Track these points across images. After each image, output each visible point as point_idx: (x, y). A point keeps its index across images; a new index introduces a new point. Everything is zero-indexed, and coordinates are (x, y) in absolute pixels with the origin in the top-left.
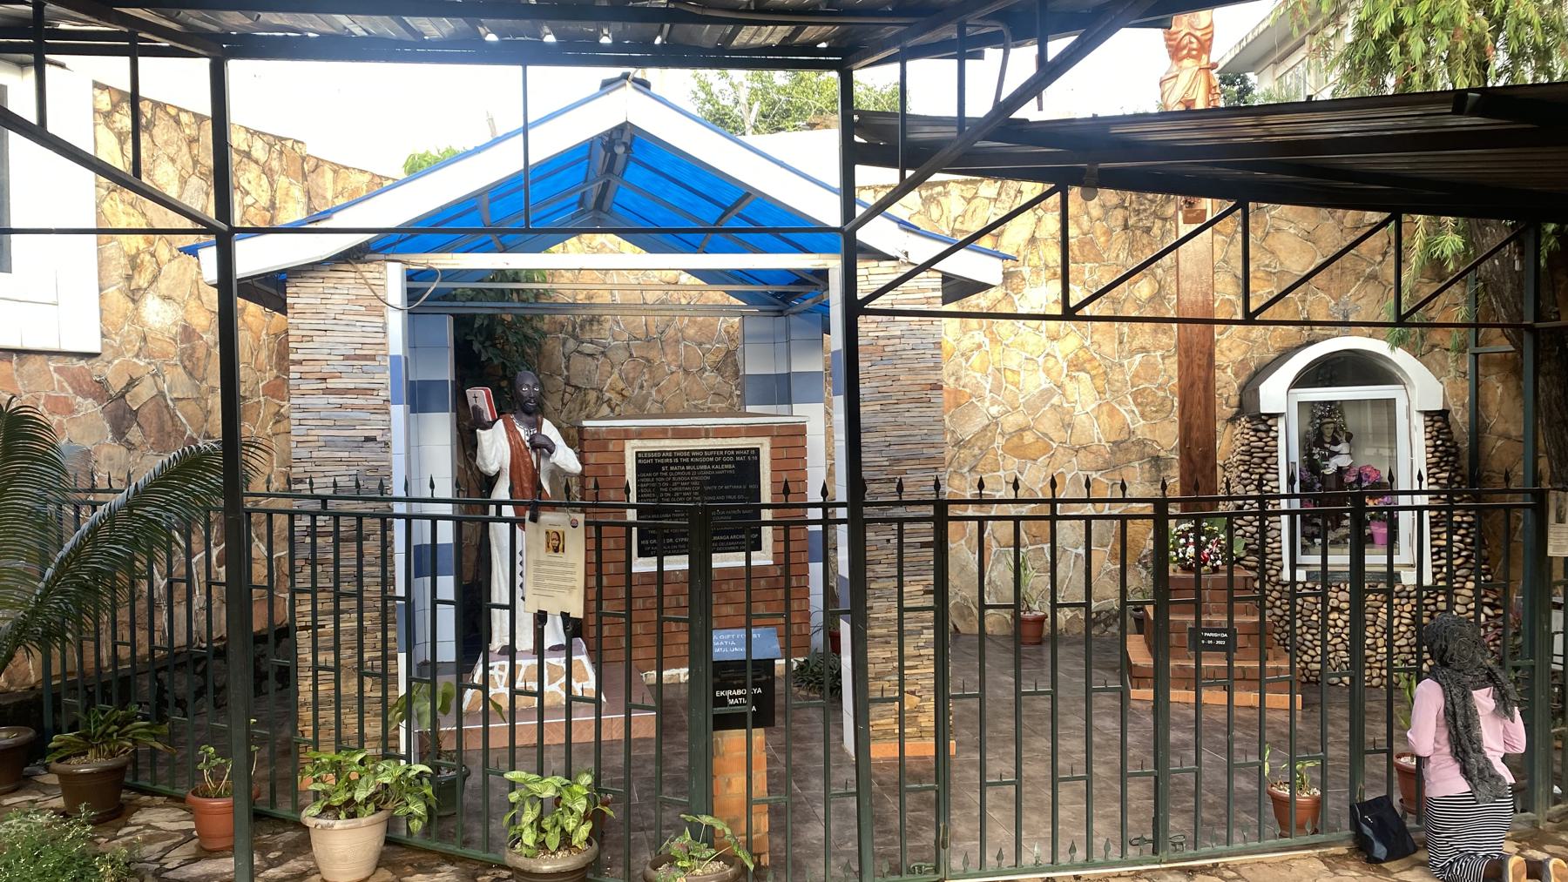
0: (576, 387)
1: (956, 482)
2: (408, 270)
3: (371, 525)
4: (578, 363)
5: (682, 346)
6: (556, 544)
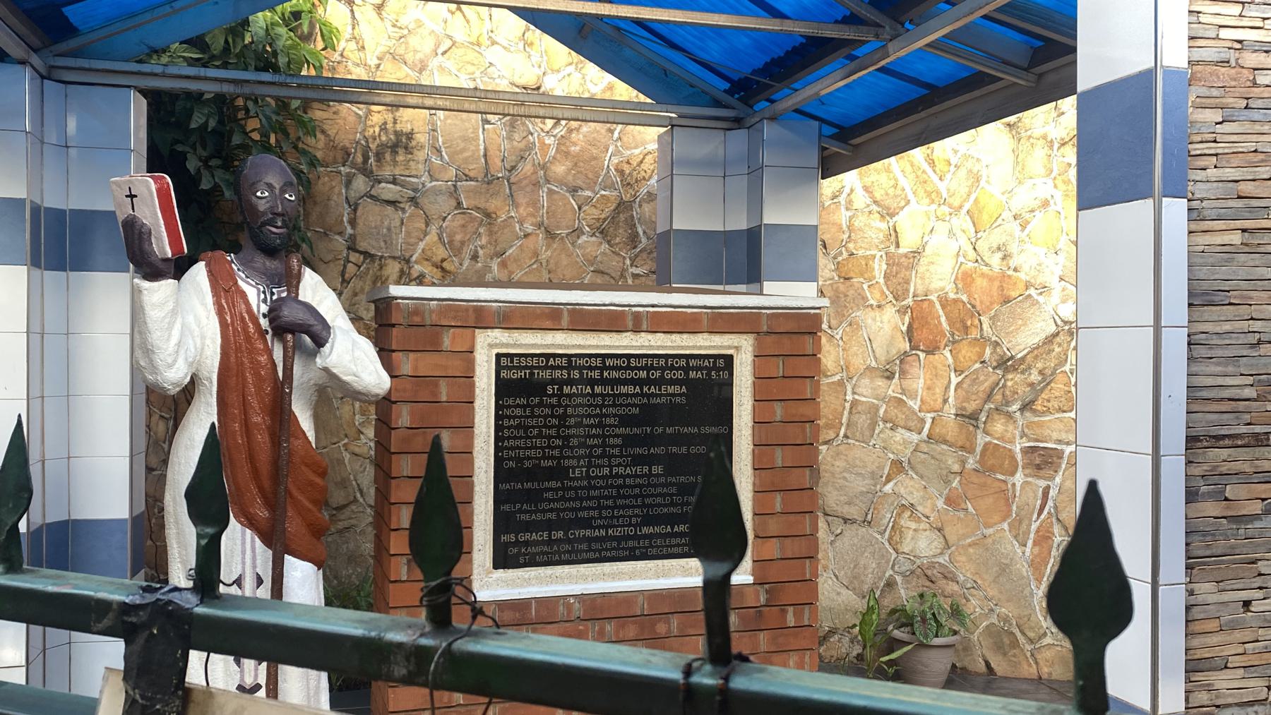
0: (366, 254)
1: (998, 426)
4: (371, 215)
5: (543, 194)
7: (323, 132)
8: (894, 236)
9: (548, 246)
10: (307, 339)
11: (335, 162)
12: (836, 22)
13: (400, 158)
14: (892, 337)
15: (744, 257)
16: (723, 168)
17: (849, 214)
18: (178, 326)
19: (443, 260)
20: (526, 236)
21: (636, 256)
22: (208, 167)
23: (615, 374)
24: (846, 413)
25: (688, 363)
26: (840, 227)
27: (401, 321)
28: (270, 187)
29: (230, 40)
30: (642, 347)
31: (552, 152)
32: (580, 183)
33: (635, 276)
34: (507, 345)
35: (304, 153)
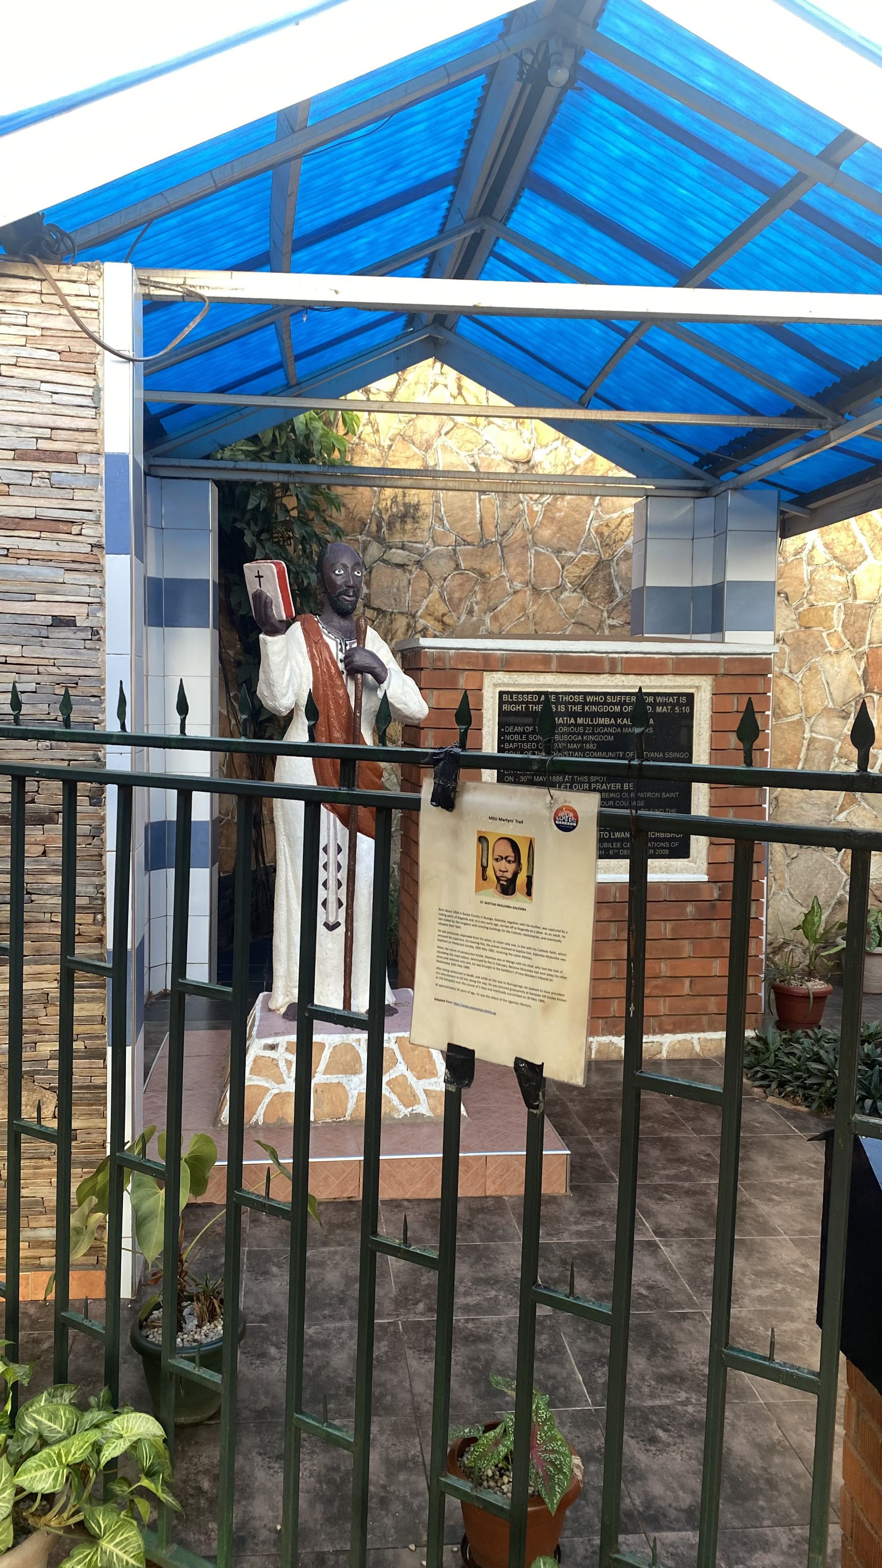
0: (379, 611)
2: (147, 296)
3: (47, 795)
4: (383, 577)
5: (531, 555)
6: (510, 872)
7: (344, 505)
8: (852, 588)
9: (535, 602)
10: (370, 677)
11: (354, 531)
12: (782, 416)
13: (408, 527)
14: (849, 681)
15: (708, 609)
16: (690, 531)
17: (810, 568)
18: (288, 667)
19: (443, 615)
20: (515, 592)
21: (613, 609)
22: (260, 541)
23: (594, 709)
24: (804, 749)
25: (655, 700)
26: (802, 580)
27: (428, 666)
28: (345, 567)
29: (277, 434)
30: (617, 686)
31: (539, 518)
32: (564, 545)
33: (612, 627)
34: (508, 685)
35: (332, 525)
